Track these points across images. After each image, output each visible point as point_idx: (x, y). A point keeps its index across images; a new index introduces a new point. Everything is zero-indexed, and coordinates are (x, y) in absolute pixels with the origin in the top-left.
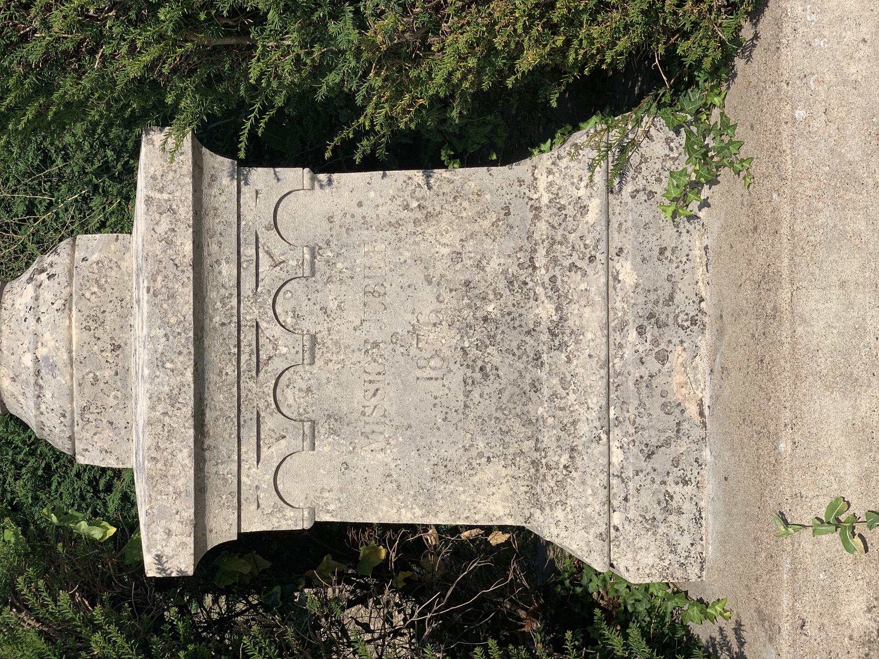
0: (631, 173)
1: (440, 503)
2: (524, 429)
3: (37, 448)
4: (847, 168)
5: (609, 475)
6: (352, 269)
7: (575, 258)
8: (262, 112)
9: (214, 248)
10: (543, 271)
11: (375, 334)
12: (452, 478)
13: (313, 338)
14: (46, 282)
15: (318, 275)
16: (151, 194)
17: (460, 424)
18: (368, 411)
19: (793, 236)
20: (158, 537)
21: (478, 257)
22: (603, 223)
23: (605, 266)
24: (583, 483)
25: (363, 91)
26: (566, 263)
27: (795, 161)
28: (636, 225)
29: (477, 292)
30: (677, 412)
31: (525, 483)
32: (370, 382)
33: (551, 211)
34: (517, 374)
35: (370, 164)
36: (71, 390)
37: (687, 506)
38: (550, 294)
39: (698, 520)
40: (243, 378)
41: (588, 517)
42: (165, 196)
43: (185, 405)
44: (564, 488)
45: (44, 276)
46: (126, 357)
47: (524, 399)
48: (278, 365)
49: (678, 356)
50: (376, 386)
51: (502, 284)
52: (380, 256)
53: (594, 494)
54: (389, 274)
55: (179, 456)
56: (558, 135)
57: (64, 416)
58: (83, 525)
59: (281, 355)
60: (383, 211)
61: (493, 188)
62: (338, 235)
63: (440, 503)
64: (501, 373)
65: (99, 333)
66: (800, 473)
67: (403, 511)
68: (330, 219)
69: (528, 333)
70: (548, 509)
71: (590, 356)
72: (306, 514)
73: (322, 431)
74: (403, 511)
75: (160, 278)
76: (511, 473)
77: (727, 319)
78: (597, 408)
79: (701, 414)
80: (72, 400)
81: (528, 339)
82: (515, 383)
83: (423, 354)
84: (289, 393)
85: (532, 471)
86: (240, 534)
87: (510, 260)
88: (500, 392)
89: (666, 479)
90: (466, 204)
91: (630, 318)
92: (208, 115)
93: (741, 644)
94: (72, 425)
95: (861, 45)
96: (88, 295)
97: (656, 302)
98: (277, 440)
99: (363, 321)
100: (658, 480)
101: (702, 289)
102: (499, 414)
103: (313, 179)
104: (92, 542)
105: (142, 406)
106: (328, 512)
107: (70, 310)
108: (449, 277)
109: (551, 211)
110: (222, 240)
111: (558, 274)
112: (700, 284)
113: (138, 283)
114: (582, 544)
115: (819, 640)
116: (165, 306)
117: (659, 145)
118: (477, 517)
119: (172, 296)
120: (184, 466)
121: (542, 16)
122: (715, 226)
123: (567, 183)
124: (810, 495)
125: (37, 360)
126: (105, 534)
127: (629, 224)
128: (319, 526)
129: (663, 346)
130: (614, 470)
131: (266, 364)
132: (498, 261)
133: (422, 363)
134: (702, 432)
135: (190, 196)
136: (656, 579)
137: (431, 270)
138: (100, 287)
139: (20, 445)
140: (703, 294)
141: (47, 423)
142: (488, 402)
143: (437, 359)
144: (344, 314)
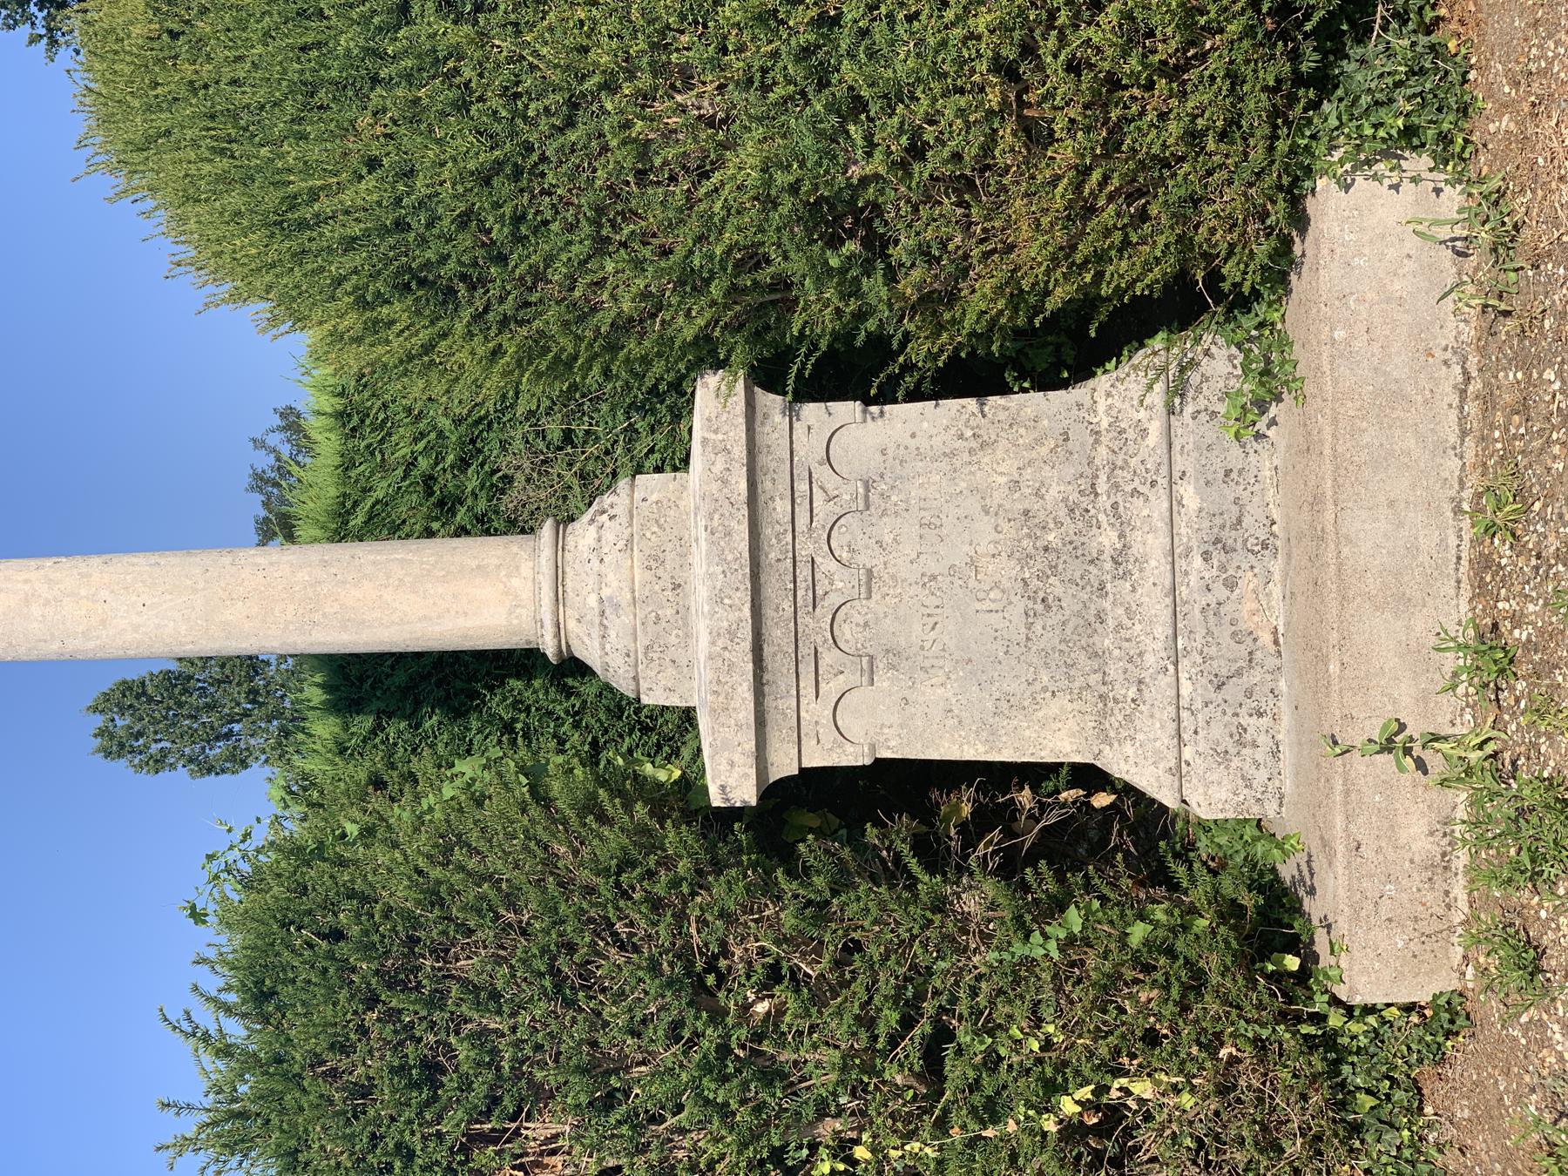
0: (1191, 394)
1: (1004, 739)
2: (1090, 662)
3: (581, 719)
4: (1394, 387)
5: (1178, 708)
6: (907, 501)
7: (1136, 483)
8: (807, 356)
9: (768, 485)
10: (1105, 498)
11: (933, 568)
12: (1015, 713)
13: (870, 573)
14: (608, 523)
15: (872, 509)
16: (707, 435)
17: (1022, 658)
18: (927, 645)
19: (1335, 457)
20: (722, 768)
21: (1037, 485)
22: (1165, 446)
23: (1168, 491)
24: (1152, 716)
25: (899, 335)
26: (1128, 489)
27: (1336, 382)
28: (1198, 448)
29: (1037, 521)
30: (1249, 640)
31: (1093, 718)
32: (929, 615)
33: (1111, 435)
34: (1081, 605)
35: (914, 396)
36: (635, 630)
37: (1263, 740)
38: (1113, 520)
39: (1275, 753)
40: (799, 614)
41: (1156, 752)
42: (720, 437)
43: (744, 640)
44: (1132, 722)
45: (605, 517)
46: (686, 596)
47: (1089, 631)
48: (834, 600)
49: (1248, 582)
50: (935, 619)
51: (1062, 513)
52: (935, 488)
53: (1162, 727)
54: (946, 505)
55: (739, 690)
56: (1125, 352)
57: (628, 656)
58: (648, 768)
59: (836, 590)
60: (937, 441)
61: (1050, 413)
62: (891, 467)
63: (1004, 739)
64: (1064, 604)
65: (660, 572)
66: (1350, 694)
67: (965, 747)
68: (883, 452)
69: (1092, 562)
70: (1116, 744)
71: (1154, 584)
72: (866, 749)
73: (881, 666)
74: (965, 747)
75: (716, 517)
76: (1078, 708)
77: (1293, 541)
78: (1163, 638)
79: (1276, 642)
80: (636, 640)
81: (1091, 568)
82: (1079, 614)
83: (981, 586)
84: (846, 627)
85: (1100, 705)
86: (801, 770)
87: (1070, 487)
88: (1064, 623)
89: (1238, 710)
90: (1022, 431)
91: (1194, 543)
92: (757, 360)
93: (1312, 875)
94: (636, 665)
95: (1405, 261)
96: (648, 535)
97: (1223, 527)
98: (835, 675)
99: (919, 554)
100: (1230, 712)
101: (1274, 511)
102: (1063, 647)
103: (865, 412)
104: (660, 785)
105: (703, 645)
106: (889, 748)
107: (632, 550)
108: (1007, 507)
109: (1111, 435)
110: (775, 476)
111: (1120, 500)
112: (1271, 506)
113: (696, 522)
114: (1152, 780)
115: (1376, 863)
116: (722, 543)
117: (1221, 363)
118: (1043, 754)
119: (728, 534)
120: (744, 699)
121: (1067, 257)
122: (1281, 445)
123: (1127, 405)
124: (1362, 716)
125: (601, 600)
126: (670, 776)
127: (1191, 446)
128: (879, 762)
129: (1231, 572)
130: (1184, 703)
131: (823, 600)
132: (1058, 489)
133: (981, 595)
134: (1278, 662)
135: (744, 436)
136: (1231, 815)
137: (988, 501)
138: (660, 526)
139: (563, 715)
140: (1275, 517)
141: (612, 664)
142: (1051, 634)
143: (996, 591)
144: (900, 547)
